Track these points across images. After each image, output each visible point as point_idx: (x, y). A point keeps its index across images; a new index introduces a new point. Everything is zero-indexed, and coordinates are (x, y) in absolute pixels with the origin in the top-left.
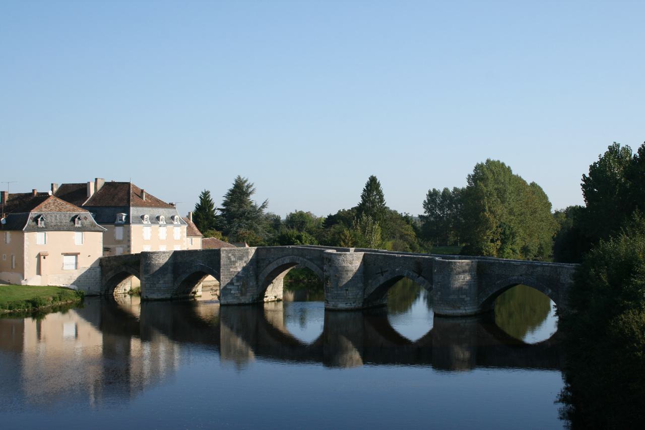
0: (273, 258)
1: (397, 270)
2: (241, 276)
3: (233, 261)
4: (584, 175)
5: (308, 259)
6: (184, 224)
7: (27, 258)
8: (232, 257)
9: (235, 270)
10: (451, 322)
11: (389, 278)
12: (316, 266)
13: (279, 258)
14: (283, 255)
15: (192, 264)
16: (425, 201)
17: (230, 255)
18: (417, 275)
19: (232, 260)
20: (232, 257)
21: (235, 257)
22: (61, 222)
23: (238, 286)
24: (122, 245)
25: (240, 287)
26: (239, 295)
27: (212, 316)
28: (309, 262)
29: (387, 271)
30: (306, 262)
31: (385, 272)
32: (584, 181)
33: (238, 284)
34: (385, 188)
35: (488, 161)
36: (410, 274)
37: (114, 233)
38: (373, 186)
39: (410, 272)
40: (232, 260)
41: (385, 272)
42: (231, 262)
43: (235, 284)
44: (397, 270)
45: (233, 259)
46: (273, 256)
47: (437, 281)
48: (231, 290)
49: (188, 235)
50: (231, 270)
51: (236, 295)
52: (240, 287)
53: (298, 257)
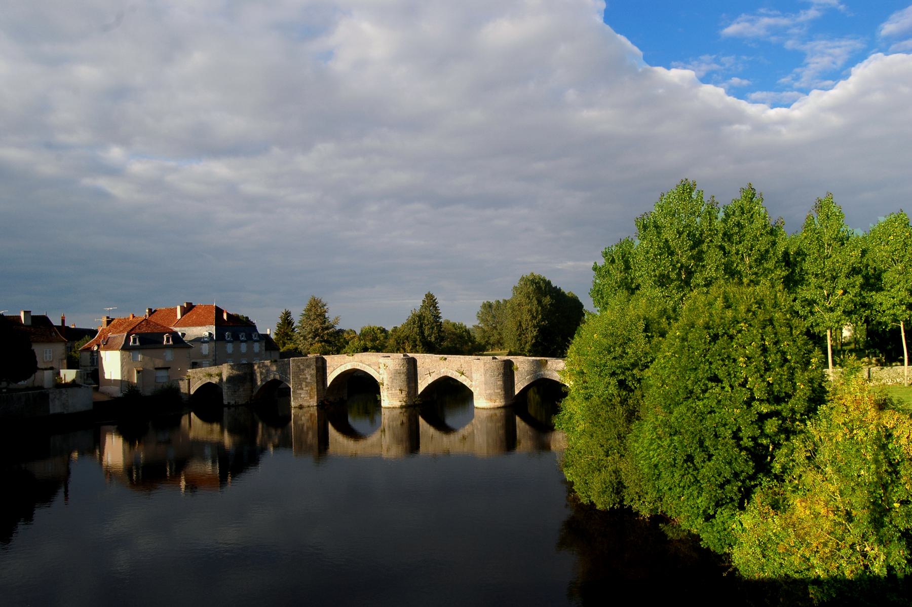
1: (442, 371)
2: (310, 381)
3: (302, 369)
6: (264, 339)
7: (429, 357)
9: (304, 377)
13: (341, 365)
14: (346, 362)
16: (478, 313)
19: (301, 368)
21: (303, 365)
23: (307, 390)
24: (208, 359)
25: (309, 391)
26: (308, 398)
28: (367, 366)
30: (365, 367)
33: (307, 389)
34: (441, 303)
35: (549, 281)
36: (453, 374)
37: (240, 347)
38: (431, 302)
39: (453, 372)
40: (301, 368)
42: (300, 370)
43: (304, 389)
44: (442, 371)
45: (302, 367)
46: (336, 363)
47: (475, 379)
48: (301, 394)
49: (266, 350)
50: (301, 377)
51: (305, 398)
52: (309, 391)
53: (358, 363)
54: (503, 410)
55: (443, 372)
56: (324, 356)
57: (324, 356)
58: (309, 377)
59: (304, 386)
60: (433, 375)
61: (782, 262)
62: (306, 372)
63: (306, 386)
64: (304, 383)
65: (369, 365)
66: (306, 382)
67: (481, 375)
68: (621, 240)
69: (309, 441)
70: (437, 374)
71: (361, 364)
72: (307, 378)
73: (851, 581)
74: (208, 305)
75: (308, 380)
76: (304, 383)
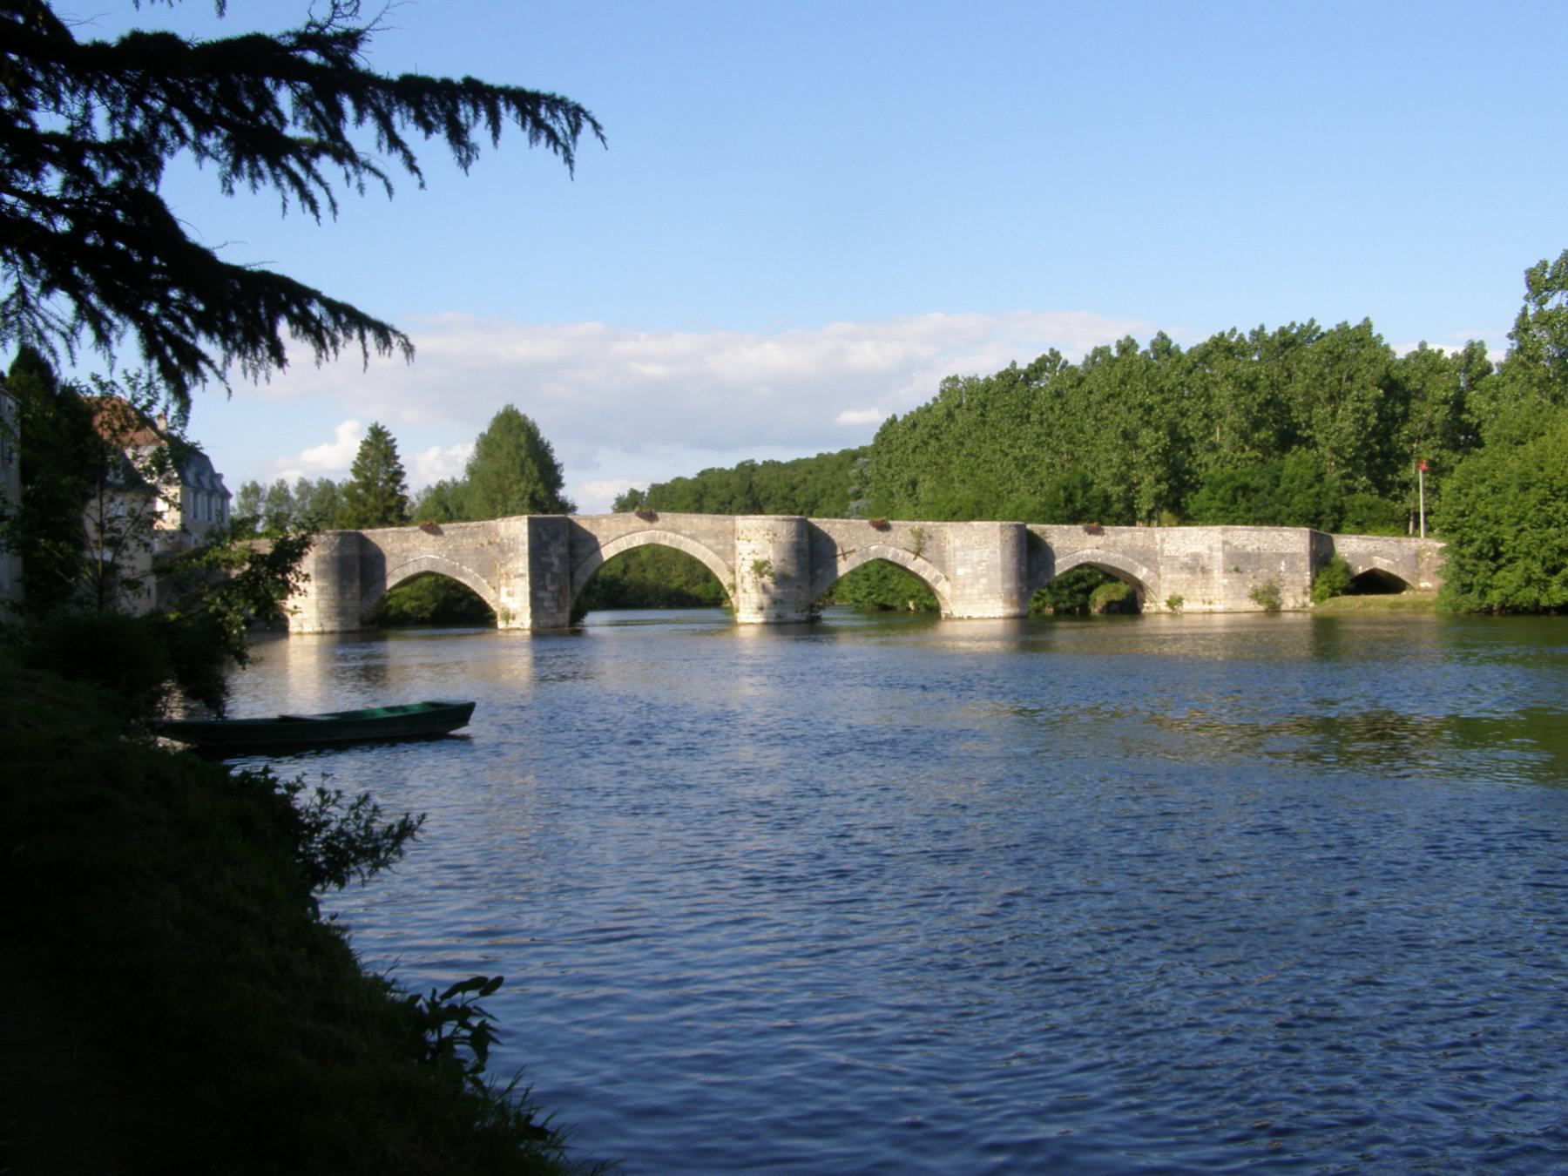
0: (607, 537)
1: (873, 548)
4: (1262, 328)
5: (685, 535)
8: (543, 534)
10: (988, 622)
11: (858, 563)
12: (704, 548)
13: (620, 537)
15: (406, 557)
17: (540, 529)
18: (913, 556)
20: (543, 534)
22: (1251, 386)
26: (555, 610)
27: (382, 686)
29: (854, 551)
30: (681, 542)
31: (850, 552)
32: (193, 359)
41: (850, 552)
44: (873, 548)
45: (545, 538)
53: (663, 533)
54: (1015, 621)
55: (876, 551)
56: (366, 532)
57: (366, 532)
58: (556, 561)
59: (548, 582)
60: (851, 557)
61: (110, 484)
62: (551, 549)
63: (553, 582)
64: (549, 576)
65: (692, 537)
66: (552, 573)
67: (995, 552)
68: (268, 379)
69: (764, 690)
70: (861, 556)
71: (670, 534)
72: (552, 564)
73: (154, 702)
74: (339, 296)
75: (555, 569)
76: (549, 576)
